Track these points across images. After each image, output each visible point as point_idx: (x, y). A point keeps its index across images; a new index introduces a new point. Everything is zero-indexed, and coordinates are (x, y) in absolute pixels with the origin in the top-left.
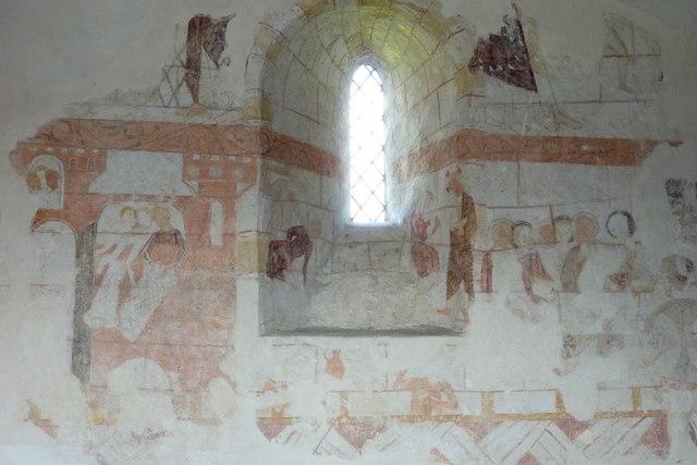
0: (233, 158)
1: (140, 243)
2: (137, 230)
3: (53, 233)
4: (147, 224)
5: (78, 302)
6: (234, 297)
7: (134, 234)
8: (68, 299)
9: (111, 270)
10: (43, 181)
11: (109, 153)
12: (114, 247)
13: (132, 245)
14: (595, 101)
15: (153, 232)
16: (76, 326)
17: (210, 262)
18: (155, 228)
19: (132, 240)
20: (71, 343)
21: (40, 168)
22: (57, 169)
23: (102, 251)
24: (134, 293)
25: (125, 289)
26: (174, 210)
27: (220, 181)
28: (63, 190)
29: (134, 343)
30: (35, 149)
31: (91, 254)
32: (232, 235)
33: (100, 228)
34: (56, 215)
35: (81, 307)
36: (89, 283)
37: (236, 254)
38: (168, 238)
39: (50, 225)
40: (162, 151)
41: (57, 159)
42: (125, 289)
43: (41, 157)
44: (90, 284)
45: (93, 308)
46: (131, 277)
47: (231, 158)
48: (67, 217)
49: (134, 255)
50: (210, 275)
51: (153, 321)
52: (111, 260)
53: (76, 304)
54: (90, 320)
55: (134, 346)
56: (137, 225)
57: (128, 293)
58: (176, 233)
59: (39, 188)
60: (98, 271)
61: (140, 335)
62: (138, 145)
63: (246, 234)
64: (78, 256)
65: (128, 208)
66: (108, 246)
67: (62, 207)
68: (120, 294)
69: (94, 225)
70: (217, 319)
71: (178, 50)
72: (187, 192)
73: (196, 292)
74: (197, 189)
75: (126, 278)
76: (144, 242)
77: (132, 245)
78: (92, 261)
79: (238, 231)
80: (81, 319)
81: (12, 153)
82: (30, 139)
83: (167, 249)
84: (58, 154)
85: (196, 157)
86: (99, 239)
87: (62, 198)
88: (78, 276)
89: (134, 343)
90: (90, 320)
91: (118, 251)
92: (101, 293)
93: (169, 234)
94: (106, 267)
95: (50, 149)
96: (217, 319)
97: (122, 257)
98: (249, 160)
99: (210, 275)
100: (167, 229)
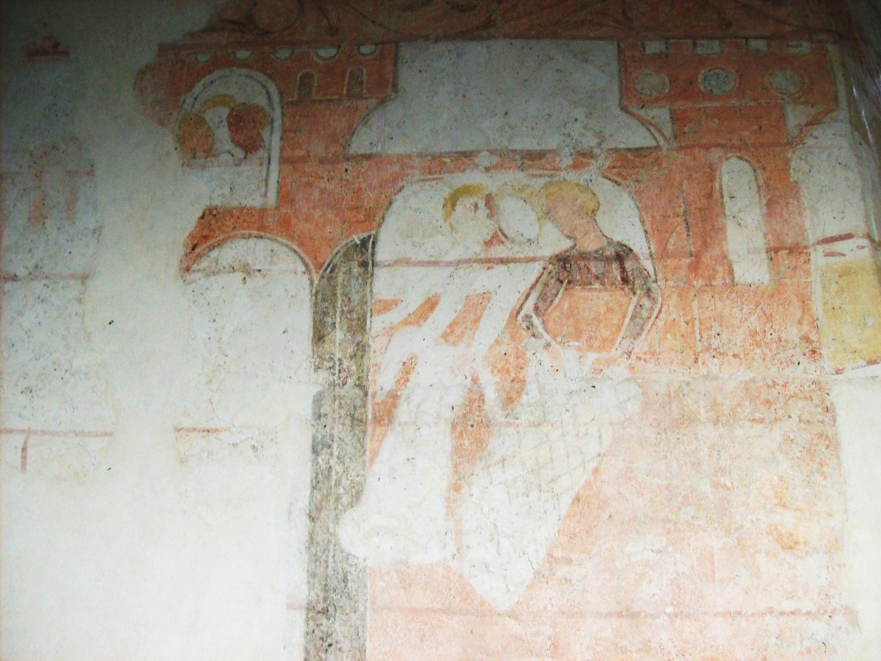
0: (761, 45)
1: (511, 286)
2: (498, 251)
3: (247, 271)
4: (531, 232)
5: (321, 480)
6: (832, 443)
7: (489, 262)
8: (291, 467)
9: (422, 377)
10: (223, 134)
11: (406, 50)
12: (431, 304)
13: (486, 296)
14: (35, 433)
15: (549, 251)
16: (315, 559)
17: (740, 336)
18: (553, 242)
19: (483, 280)
20: (299, 617)
21: (221, 100)
22: (262, 101)
23: (394, 316)
24: (500, 443)
25: (471, 427)
26: (608, 185)
27: (734, 102)
28: (275, 154)
29: (512, 615)
30: (202, 58)
31: (358, 326)
32: (797, 250)
33: (383, 253)
34: (253, 222)
35: (330, 494)
36: (354, 414)
37: (818, 308)
38: (596, 268)
39: (234, 251)
40: (554, 36)
41: (261, 77)
42: (471, 427)
43: (216, 74)
44: (357, 421)
45: (369, 496)
46: (490, 394)
47: (754, 44)
48: (285, 225)
49: (493, 323)
50: (744, 375)
51: (573, 536)
52: (422, 341)
53: (315, 486)
54: (354, 535)
55: (514, 627)
56: (498, 237)
57: (479, 442)
58: (622, 254)
59: (210, 152)
60: (383, 380)
61: (531, 586)
62: (488, 24)
63: (839, 246)
64: (319, 337)
65: (466, 191)
66: (413, 302)
67: (272, 198)
68: (458, 450)
69: (366, 246)
70: (787, 520)
71: (451, 269)
72: (640, 138)
73: (708, 433)
74: (668, 129)
75: (474, 400)
76: (524, 287)
77: (486, 296)
78: (361, 350)
79: (812, 237)
80: (332, 540)
81: (142, 73)
82: (192, 35)
83: (596, 300)
84: (265, 66)
85: (654, 47)
86: (384, 284)
87: (274, 177)
88: (318, 400)
89: (512, 615)
90: (354, 535)
91: (442, 317)
92: (390, 448)
93: (599, 256)
94: (408, 368)
95: (243, 54)
96: (787, 520)
97: (450, 334)
98: (805, 47)
99: (744, 375)
100: (590, 244)
